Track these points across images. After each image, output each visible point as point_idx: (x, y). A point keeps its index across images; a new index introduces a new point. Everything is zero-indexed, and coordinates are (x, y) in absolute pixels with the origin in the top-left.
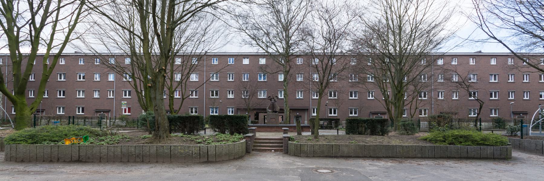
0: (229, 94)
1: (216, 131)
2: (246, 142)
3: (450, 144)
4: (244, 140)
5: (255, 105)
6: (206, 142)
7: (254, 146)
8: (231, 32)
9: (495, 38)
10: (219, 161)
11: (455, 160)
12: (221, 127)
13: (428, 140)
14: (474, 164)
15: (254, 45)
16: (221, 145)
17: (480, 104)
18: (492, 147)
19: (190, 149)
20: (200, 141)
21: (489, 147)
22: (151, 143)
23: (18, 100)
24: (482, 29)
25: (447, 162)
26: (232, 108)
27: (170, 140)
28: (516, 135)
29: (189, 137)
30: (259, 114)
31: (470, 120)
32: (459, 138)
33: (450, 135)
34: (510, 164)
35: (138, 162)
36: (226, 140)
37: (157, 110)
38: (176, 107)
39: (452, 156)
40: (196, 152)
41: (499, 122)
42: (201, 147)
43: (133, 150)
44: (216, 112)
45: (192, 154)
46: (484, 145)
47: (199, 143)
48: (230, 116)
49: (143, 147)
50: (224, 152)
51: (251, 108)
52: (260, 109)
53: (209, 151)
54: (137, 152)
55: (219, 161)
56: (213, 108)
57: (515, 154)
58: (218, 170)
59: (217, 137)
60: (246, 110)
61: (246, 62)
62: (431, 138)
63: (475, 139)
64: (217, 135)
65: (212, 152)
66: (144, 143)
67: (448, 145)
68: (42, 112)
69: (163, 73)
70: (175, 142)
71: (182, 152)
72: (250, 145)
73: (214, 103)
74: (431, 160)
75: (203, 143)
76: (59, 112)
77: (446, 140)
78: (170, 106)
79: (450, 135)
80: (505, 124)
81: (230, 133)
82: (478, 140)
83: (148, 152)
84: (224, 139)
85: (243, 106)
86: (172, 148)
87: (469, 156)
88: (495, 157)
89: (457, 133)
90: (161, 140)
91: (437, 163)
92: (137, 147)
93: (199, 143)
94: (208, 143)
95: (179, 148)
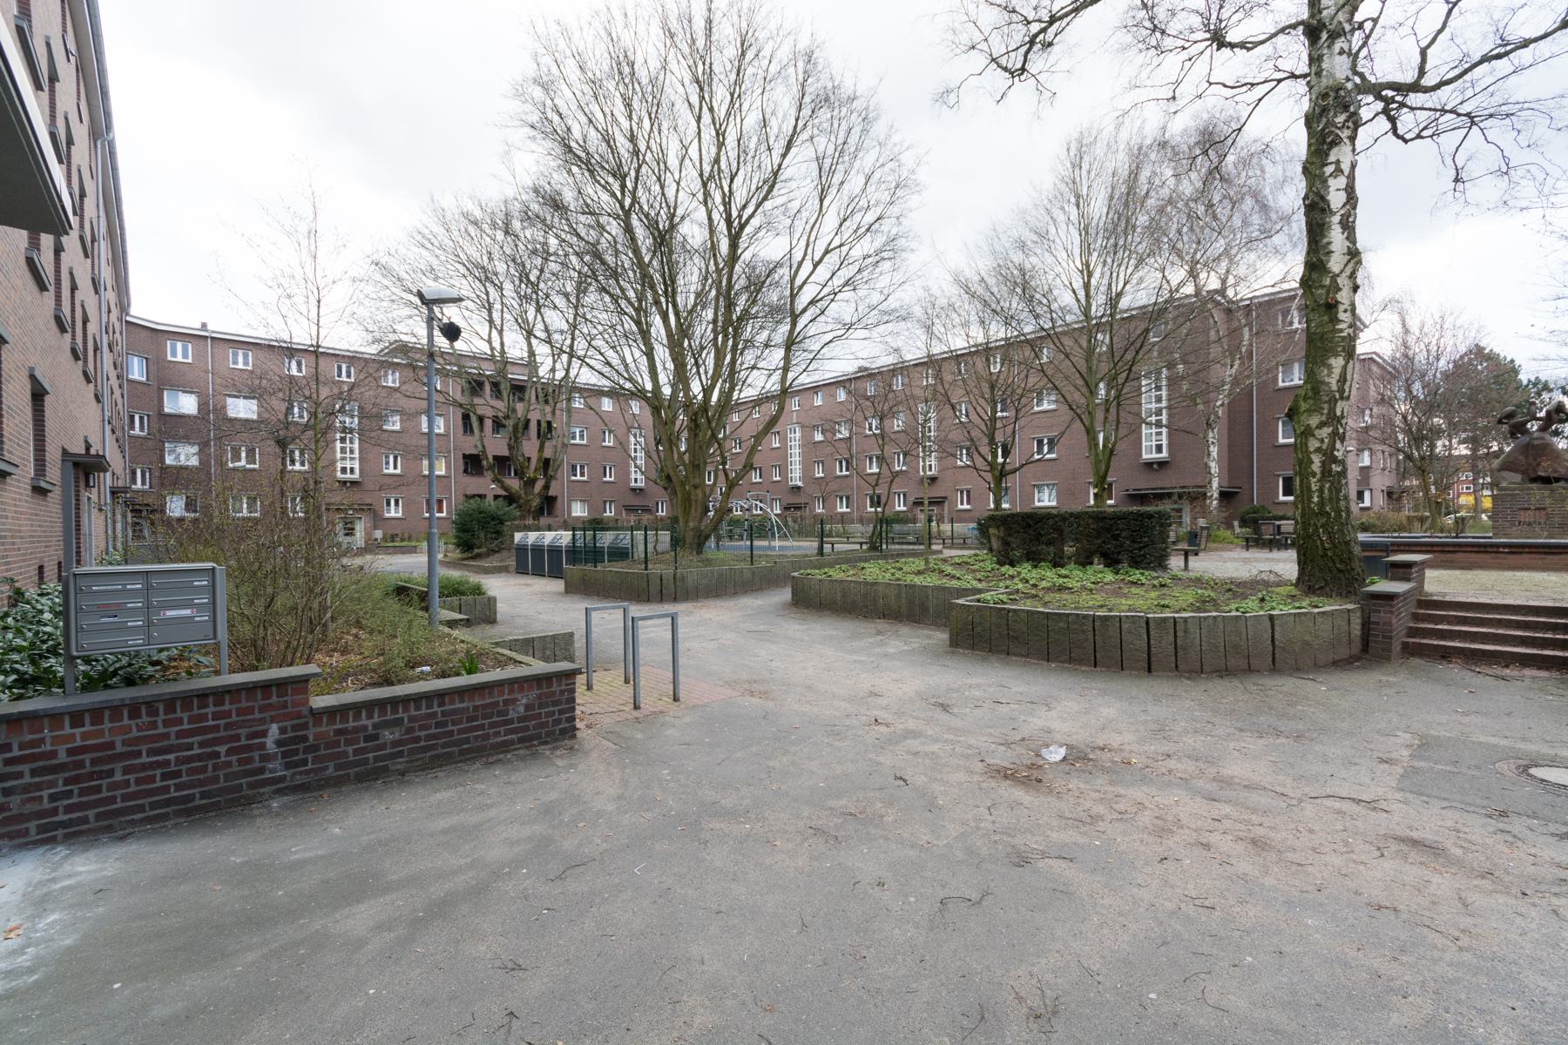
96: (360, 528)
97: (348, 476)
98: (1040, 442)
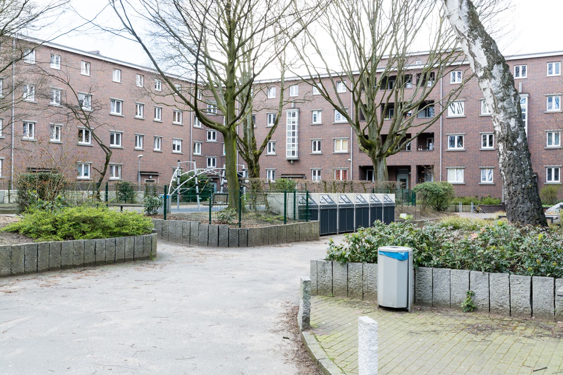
3: (65, 238)
9: (134, 34)
11: (75, 270)
13: (21, 232)
14: (107, 274)
17: (105, 155)
18: (132, 238)
21: (128, 238)
24: (114, 8)
25: (62, 277)
28: (155, 214)
30: (394, 194)
31: (84, 186)
32: (82, 224)
33: (65, 218)
34: (158, 267)
39: (69, 264)
41: (126, 191)
46: (120, 234)
57: (162, 248)
62: (28, 227)
63: (107, 224)
67: (63, 241)
74: (31, 277)
77: (57, 229)
79: (65, 218)
80: (133, 194)
82: (112, 226)
87: (98, 259)
88: (135, 256)
89: (78, 214)
91: (44, 282)
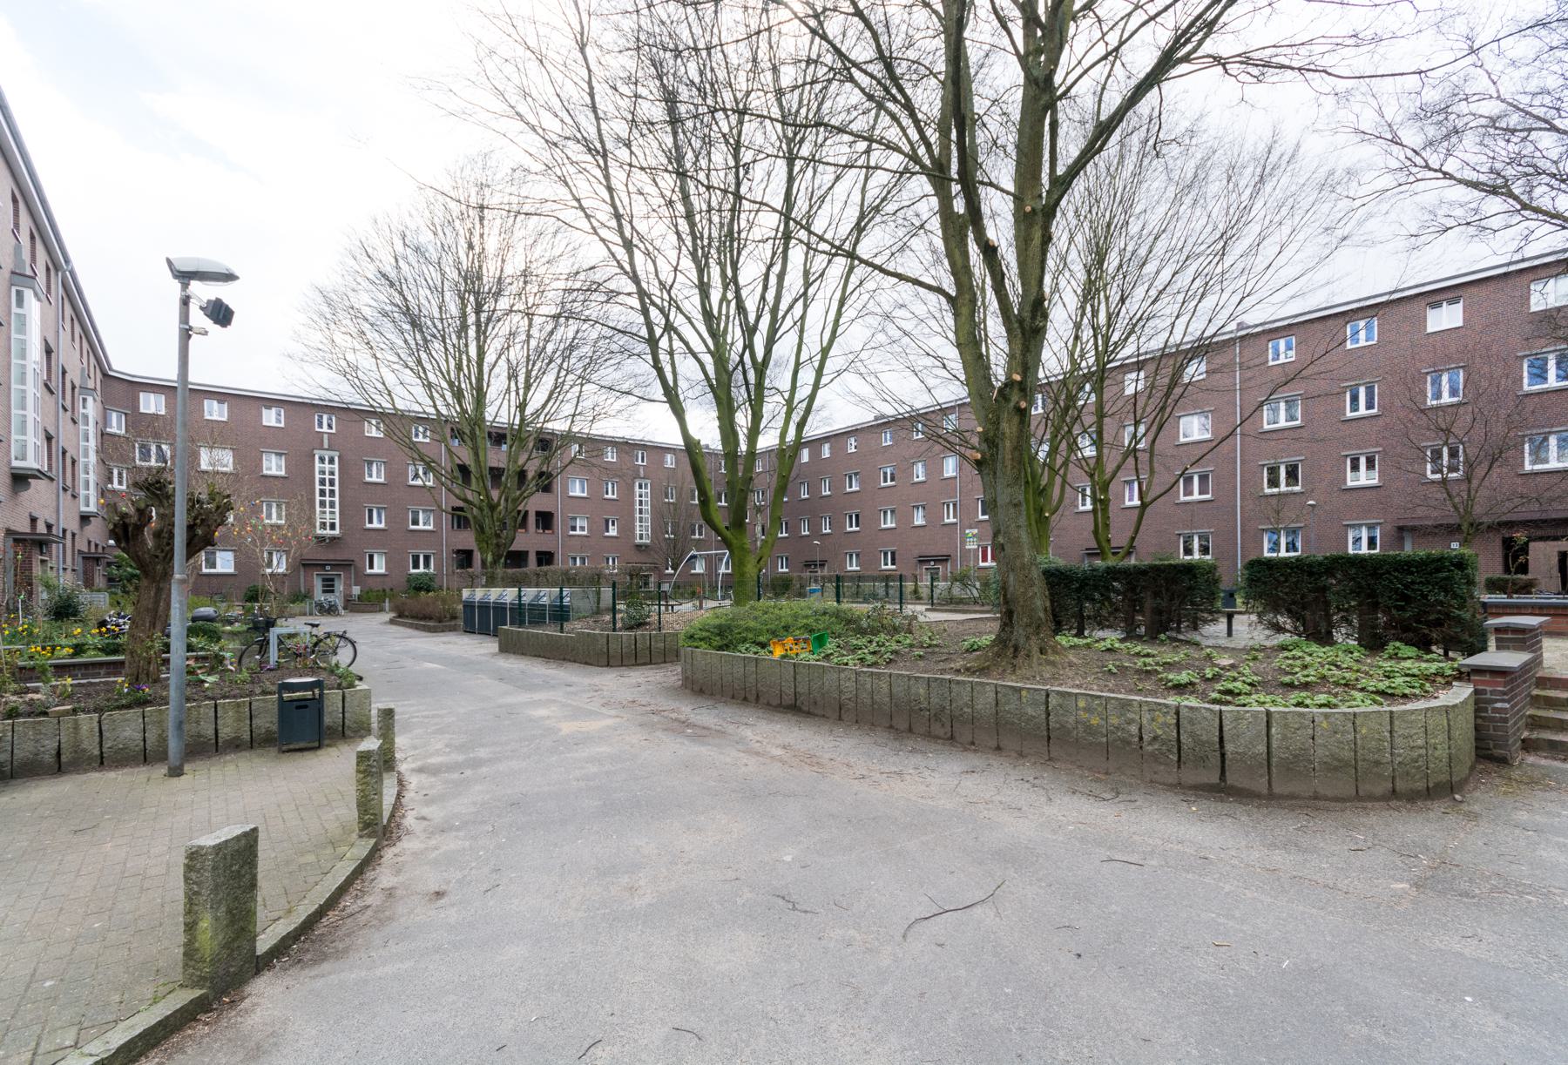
0: (1355, 468)
1: (1279, 629)
2: (1476, 702)
4: (1460, 693)
5: (1509, 505)
6: (1218, 686)
7: (1536, 723)
8: (1358, 203)
10: (1292, 797)
12: (1307, 614)
15: (1495, 223)
16: (1302, 715)
19: (1130, 715)
20: (1184, 677)
22: (983, 671)
23: (735, 541)
26: (1371, 527)
27: (1053, 664)
29: (1138, 654)
35: (938, 737)
36: (1337, 684)
37: (1002, 547)
38: (1119, 537)
40: (1159, 732)
42: (1183, 712)
43: (922, 691)
44: (1291, 547)
45: (1141, 738)
47: (1180, 688)
48: (1358, 561)
49: (953, 686)
50: (1320, 752)
51: (1485, 519)
52: (1545, 521)
53: (1226, 736)
54: (935, 700)
55: (1292, 797)
56: (1276, 531)
58: (1278, 857)
59: (1279, 660)
60: (1452, 530)
61: (1446, 318)
64: (1283, 648)
65: (1244, 742)
66: (958, 671)
68: (822, 565)
69: (1015, 397)
70: (1071, 674)
71: (1093, 722)
72: (1505, 720)
73: (1278, 512)
75: (1201, 687)
76: (851, 565)
78: (1096, 532)
81: (1359, 640)
83: (967, 705)
84: (1324, 677)
85: (1429, 515)
86: (1053, 701)
90: (1019, 661)
92: (933, 685)
93: (1180, 688)
94: (1229, 692)
95: (1082, 704)
96: (340, 587)
97: (328, 532)
98: (1273, 471)
